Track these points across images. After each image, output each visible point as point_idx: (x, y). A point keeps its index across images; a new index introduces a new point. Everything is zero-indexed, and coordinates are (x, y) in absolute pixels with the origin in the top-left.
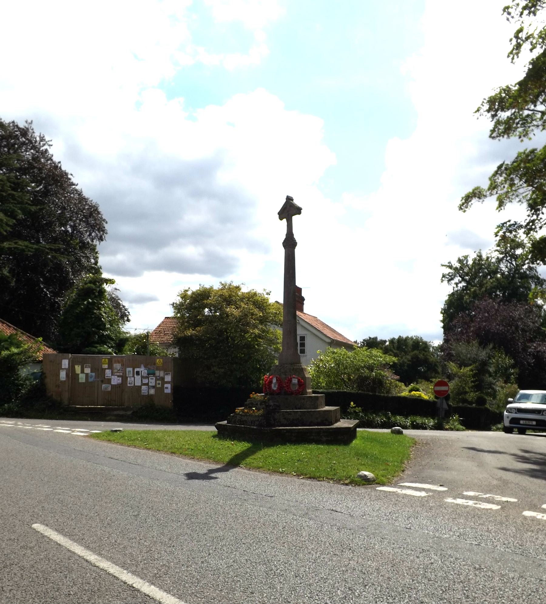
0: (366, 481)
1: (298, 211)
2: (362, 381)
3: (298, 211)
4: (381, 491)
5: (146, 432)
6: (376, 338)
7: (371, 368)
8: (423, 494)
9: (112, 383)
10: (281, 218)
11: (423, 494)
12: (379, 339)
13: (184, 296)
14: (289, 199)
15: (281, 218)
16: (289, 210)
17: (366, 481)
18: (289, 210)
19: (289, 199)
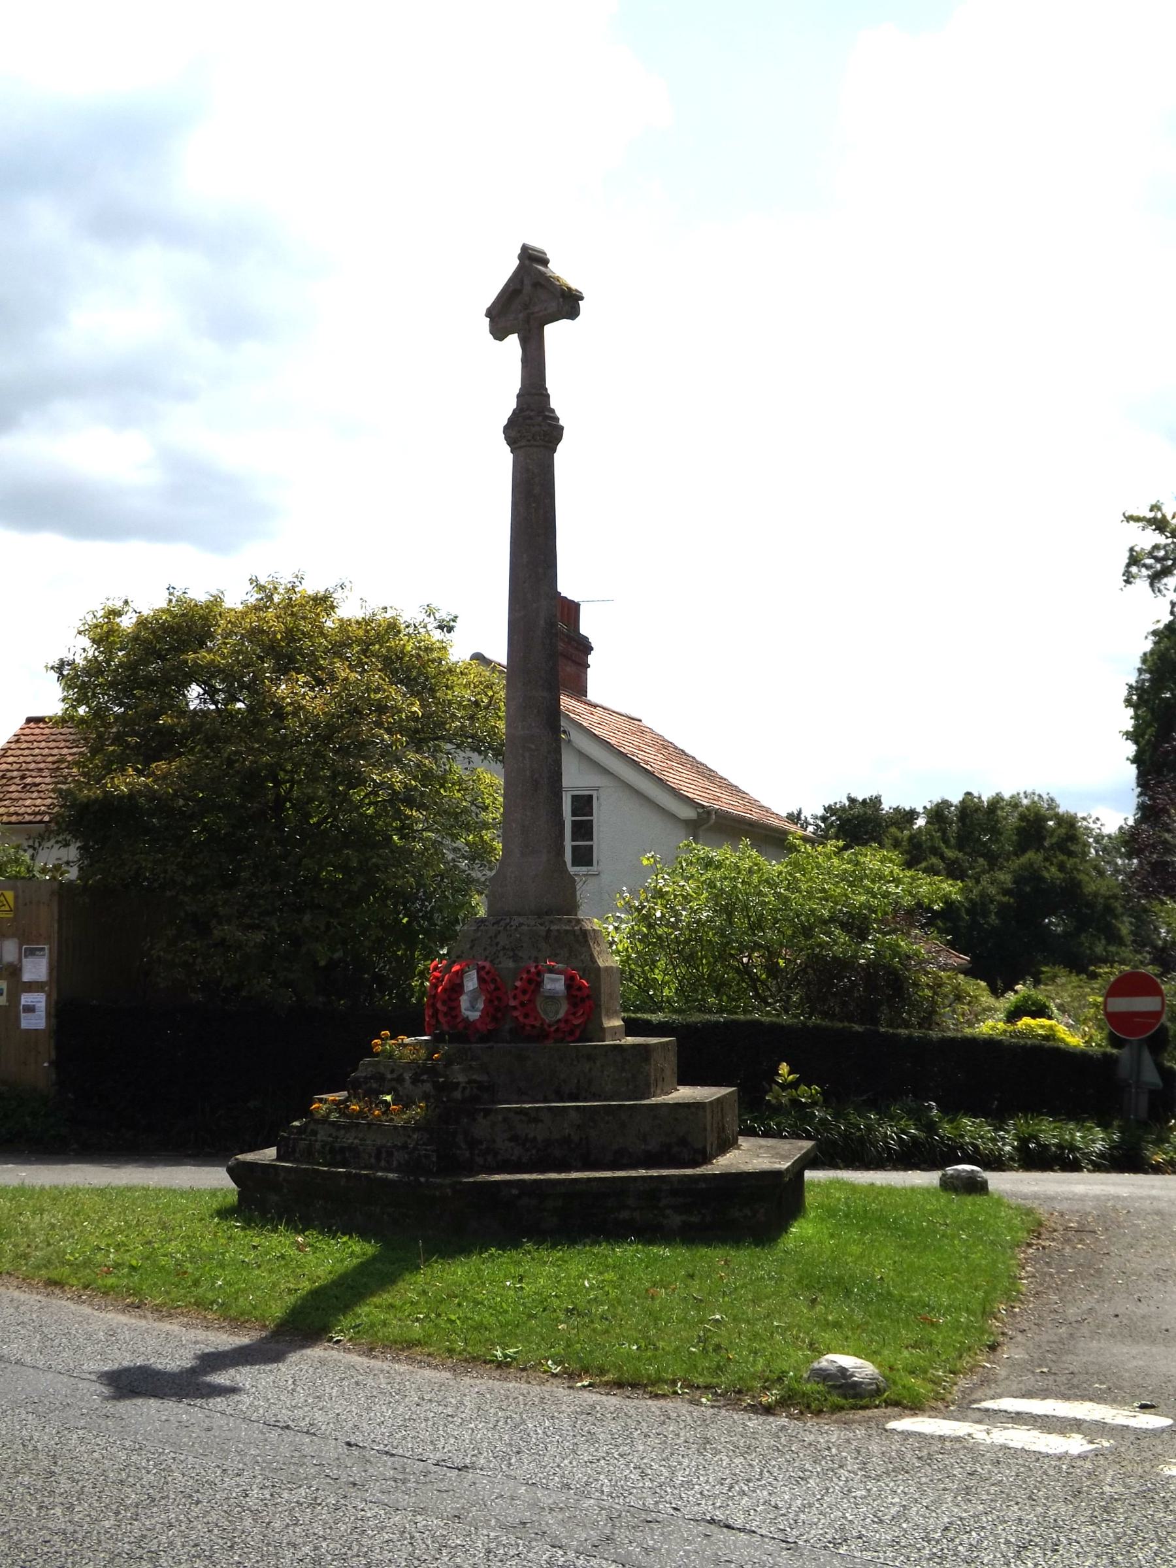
0: (846, 1395)
1: (568, 303)
2: (823, 974)
3: (568, 303)
4: (906, 1435)
6: (876, 802)
8: (1076, 1444)
10: (499, 334)
11: (1076, 1444)
12: (887, 805)
13: (104, 634)
14: (531, 259)
15: (499, 334)
16: (532, 302)
17: (846, 1395)
18: (532, 302)
19: (531, 259)
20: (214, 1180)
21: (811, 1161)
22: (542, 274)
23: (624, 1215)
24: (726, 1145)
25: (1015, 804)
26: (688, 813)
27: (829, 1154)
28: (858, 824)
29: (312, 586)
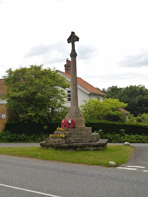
0: (111, 166)
1: (78, 39)
2: (110, 117)
3: (78, 39)
4: (118, 169)
5: (117, 146)
6: (116, 87)
7: (113, 110)
8: (135, 169)
9: (108, 144)
10: (69, 43)
11: (135, 169)
12: (118, 87)
13: (10, 71)
14: (73, 33)
15: (69, 43)
16: (73, 38)
17: (111, 166)
18: (73, 38)
19: (73, 33)
20: (37, 145)
21: (108, 142)
22: (74, 35)
23: (87, 148)
24: (98, 140)
25: (138, 87)
26: (89, 93)
27: (110, 141)
28: (114, 92)
29: (38, 65)
